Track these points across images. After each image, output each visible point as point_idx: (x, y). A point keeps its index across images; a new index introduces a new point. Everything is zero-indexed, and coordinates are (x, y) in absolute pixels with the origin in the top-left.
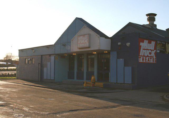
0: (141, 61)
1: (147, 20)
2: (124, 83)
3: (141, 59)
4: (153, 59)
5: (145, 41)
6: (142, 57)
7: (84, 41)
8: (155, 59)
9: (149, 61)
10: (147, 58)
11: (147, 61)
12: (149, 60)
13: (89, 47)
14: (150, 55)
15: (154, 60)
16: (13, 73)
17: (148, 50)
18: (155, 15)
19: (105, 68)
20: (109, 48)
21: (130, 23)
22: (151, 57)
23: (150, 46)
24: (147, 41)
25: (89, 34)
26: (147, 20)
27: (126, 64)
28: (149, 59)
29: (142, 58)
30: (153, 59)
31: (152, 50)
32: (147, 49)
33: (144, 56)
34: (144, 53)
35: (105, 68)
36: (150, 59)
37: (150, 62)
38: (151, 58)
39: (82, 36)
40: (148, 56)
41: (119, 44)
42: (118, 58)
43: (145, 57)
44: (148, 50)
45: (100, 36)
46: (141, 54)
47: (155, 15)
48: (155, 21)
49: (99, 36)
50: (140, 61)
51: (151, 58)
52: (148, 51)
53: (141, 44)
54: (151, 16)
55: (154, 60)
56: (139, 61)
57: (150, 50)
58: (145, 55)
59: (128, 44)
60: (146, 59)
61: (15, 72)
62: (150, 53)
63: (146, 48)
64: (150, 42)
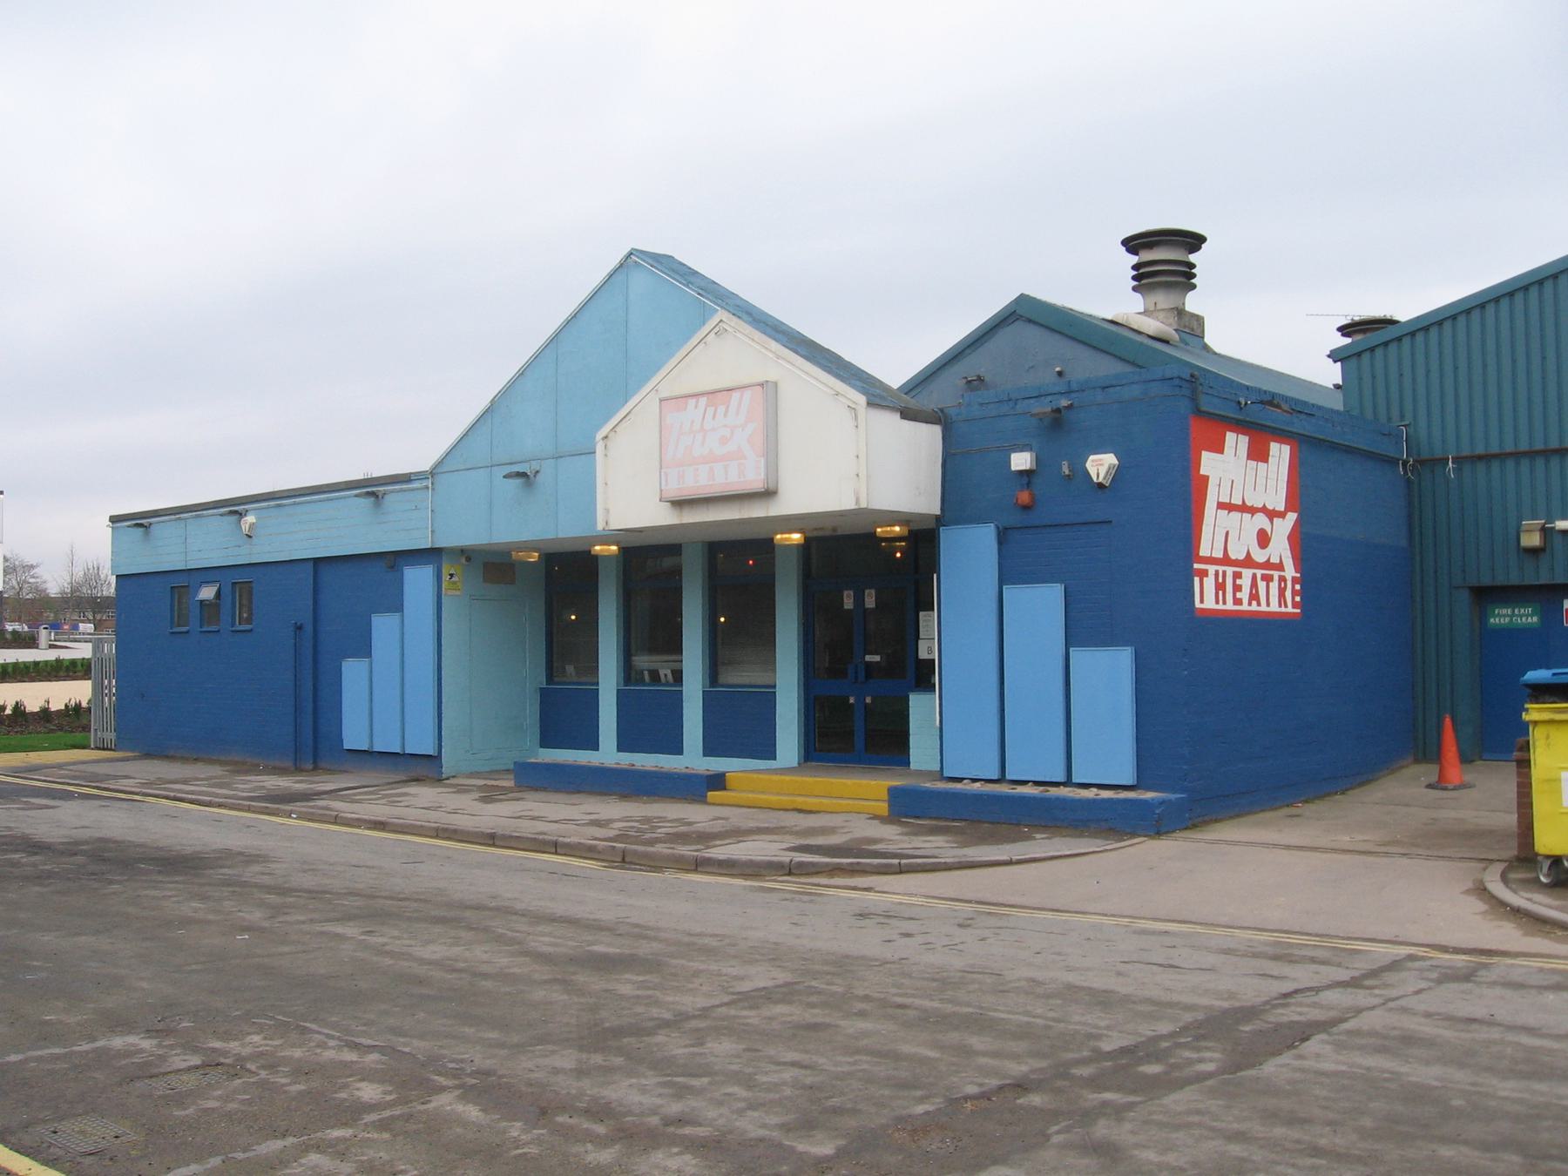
0: (1209, 603)
1: (1134, 278)
2: (1068, 783)
3: (1209, 583)
4: (1282, 579)
5: (1230, 437)
6: (1212, 569)
7: (724, 441)
8: (1294, 580)
9: (1259, 604)
10: (1247, 574)
11: (1245, 601)
12: (1254, 596)
13: (768, 494)
14: (1259, 556)
15: (1288, 594)
16: (79, 692)
17: (1252, 511)
18: (1194, 241)
19: (868, 658)
20: (935, 509)
21: (1023, 299)
22: (1267, 565)
23: (1261, 481)
24: (1244, 440)
25: (761, 385)
26: (1134, 278)
27: (1082, 629)
28: (1254, 584)
29: (1217, 573)
30: (1282, 579)
31: (1272, 515)
32: (1243, 508)
33: (1226, 560)
34: (1227, 533)
35: (868, 658)
36: (1262, 585)
37: (1264, 608)
38: (1267, 579)
39: (703, 400)
40: (1248, 562)
41: (1021, 461)
42: (1009, 574)
43: (1230, 570)
44: (1252, 511)
45: (870, 404)
46: (1204, 551)
47: (1194, 241)
48: (1194, 287)
49: (861, 399)
50: (1202, 601)
51: (1267, 579)
52: (1247, 516)
53: (1209, 463)
54: (1147, 256)
55: (1288, 594)
56: (1198, 604)
57: (1264, 510)
58: (1233, 557)
59: (1100, 465)
60: (1237, 588)
61: (79, 692)
62: (1263, 539)
63: (1237, 501)
64: (1258, 453)
